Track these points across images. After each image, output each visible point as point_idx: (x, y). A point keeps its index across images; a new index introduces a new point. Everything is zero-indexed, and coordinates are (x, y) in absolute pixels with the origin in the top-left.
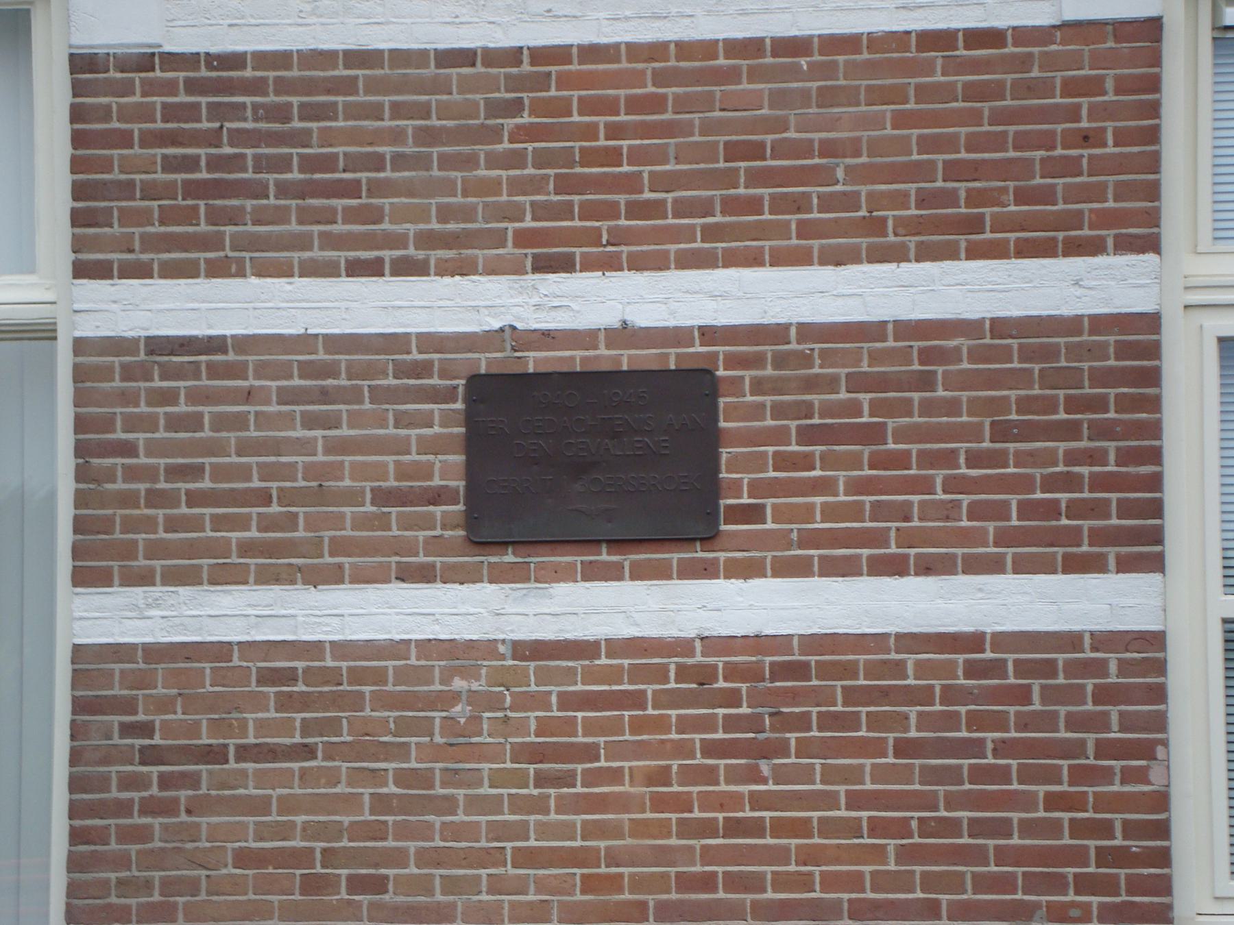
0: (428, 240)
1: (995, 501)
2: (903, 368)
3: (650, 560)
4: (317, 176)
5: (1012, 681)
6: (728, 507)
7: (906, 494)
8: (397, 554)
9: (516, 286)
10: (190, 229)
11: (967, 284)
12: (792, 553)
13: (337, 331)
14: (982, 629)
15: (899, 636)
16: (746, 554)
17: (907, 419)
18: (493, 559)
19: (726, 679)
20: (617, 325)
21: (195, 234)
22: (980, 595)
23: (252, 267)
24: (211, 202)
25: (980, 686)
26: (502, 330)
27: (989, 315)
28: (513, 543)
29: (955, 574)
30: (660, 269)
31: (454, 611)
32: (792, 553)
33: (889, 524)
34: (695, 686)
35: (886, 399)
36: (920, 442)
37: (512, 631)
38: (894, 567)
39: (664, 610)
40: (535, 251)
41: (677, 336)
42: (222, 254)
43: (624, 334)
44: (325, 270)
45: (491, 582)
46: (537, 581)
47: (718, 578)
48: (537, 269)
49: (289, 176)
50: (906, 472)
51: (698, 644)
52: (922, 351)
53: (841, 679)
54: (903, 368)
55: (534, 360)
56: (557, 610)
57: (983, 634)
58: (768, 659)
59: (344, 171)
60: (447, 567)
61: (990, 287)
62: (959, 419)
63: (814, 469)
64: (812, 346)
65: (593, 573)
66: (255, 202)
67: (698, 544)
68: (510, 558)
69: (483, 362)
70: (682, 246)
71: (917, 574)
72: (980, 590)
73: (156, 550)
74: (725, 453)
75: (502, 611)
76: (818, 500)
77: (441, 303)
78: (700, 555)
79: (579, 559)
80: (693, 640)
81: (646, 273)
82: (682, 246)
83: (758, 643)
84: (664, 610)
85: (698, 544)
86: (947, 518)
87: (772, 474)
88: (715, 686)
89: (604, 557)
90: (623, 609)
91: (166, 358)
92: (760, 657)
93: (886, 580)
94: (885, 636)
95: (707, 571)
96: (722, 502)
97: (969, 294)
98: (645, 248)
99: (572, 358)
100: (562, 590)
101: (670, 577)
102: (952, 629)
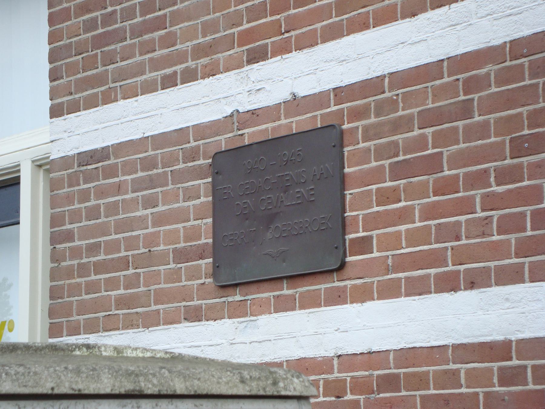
0: (200, 51)
1: (515, 214)
2: (452, 101)
3: (308, 291)
4: (148, 17)
5: (531, 387)
6: (351, 240)
7: (457, 215)
8: (184, 300)
9: (239, 77)
10: (94, 72)
11: (494, 13)
12: (389, 277)
13: (156, 132)
14: (509, 337)
15: (456, 347)
16: (361, 281)
17: (456, 147)
18: (230, 299)
19: (352, 393)
20: (289, 98)
21: (97, 74)
22: (507, 305)
23: (121, 93)
24: (103, 49)
25: (510, 393)
26: (232, 115)
27: (508, 39)
28: (287, 278)
29: (490, 286)
30: (312, 46)
31: (210, 343)
32: (389, 277)
33: (446, 244)
34: (333, 399)
35: (442, 130)
36: (464, 166)
37: (239, 357)
38: (449, 284)
39: (316, 333)
40: (247, 47)
41: (318, 100)
42: (107, 87)
43: (295, 104)
44: (149, 88)
45: (229, 318)
46: (252, 315)
47: (347, 303)
48: (250, 62)
49: (135, 21)
50: (456, 195)
51: (335, 362)
52: (467, 81)
53: (418, 390)
54: (452, 101)
55: (250, 134)
56: (260, 338)
57: (511, 341)
58: (376, 373)
59: (160, 10)
60: (210, 307)
61: (509, 12)
62: (489, 141)
63: (400, 201)
64: (397, 92)
65: (284, 305)
66: (121, 44)
67: (285, 282)
68: (238, 298)
69: (223, 141)
70: (325, 23)
71: (466, 289)
72: (507, 300)
73: (83, 308)
74: (206, 199)
75: (233, 342)
76: (403, 228)
77: (204, 100)
78: (337, 284)
79: (272, 294)
80: (332, 358)
81: (305, 51)
82: (325, 23)
83: (372, 358)
84: (316, 333)
85: (335, 274)
86: (483, 235)
87: (376, 209)
88: (345, 398)
89: (286, 292)
90: (294, 335)
91: (85, 168)
92: (371, 372)
93: (446, 295)
94: (443, 348)
95: (337, 298)
96: (347, 237)
97: (495, 22)
98: (304, 30)
99: (267, 129)
100: (264, 320)
101: (320, 306)
102: (488, 339)
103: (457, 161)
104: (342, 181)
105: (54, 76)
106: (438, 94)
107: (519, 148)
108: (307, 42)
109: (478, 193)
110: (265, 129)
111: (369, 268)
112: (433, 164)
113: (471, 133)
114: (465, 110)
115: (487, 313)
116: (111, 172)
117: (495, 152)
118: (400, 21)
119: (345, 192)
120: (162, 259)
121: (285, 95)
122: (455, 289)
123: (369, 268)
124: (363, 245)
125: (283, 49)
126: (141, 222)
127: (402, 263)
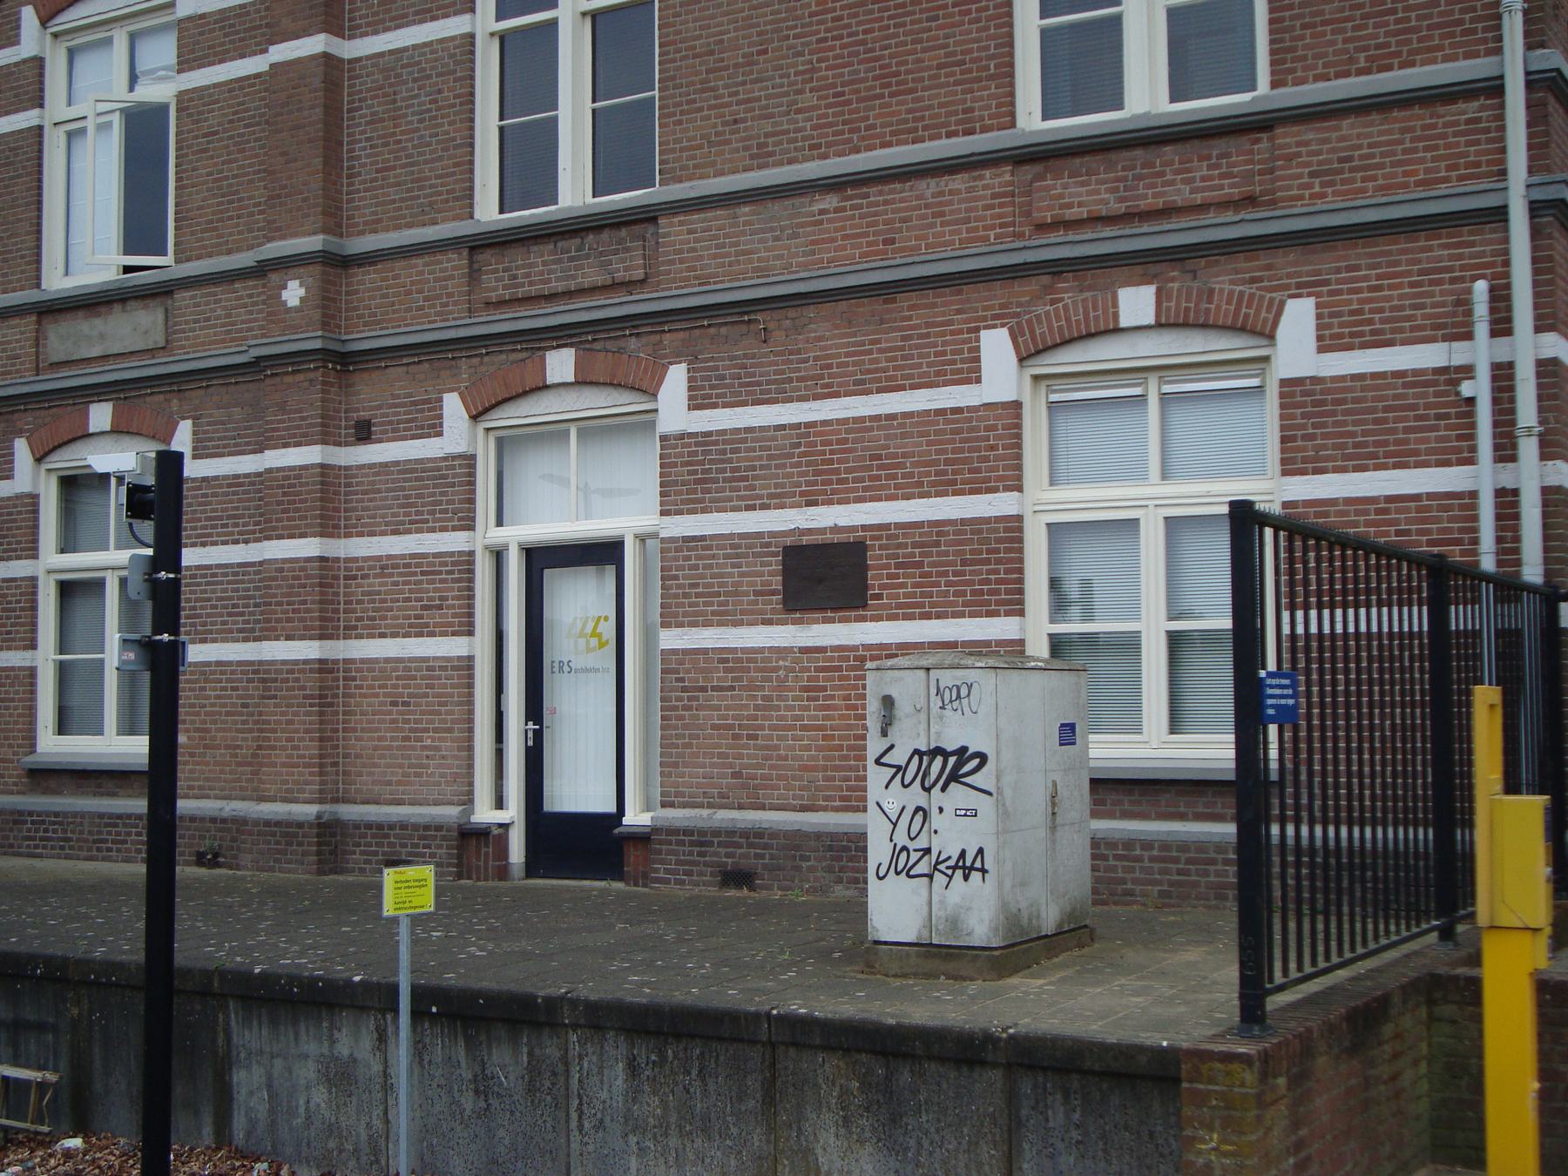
41: (853, 529)
43: (836, 529)
55: (805, 540)
69: (788, 541)
73: (685, 614)
74: (870, 573)
95: (863, 619)
103: (931, 565)
104: (865, 568)
105: (662, 494)
106: (921, 535)
107: (964, 563)
108: (846, 501)
109: (943, 580)
110: (819, 539)
111: (882, 607)
112: (920, 565)
113: (939, 554)
114: (937, 544)
115: (890, 663)
116: (709, 548)
117: (953, 563)
118: (1551, 902)
119: (150, 552)
120: (747, 594)
121: (831, 524)
122: (930, 618)
123: (882, 607)
124: (878, 597)
125: (830, 503)
126: (731, 575)
127: (899, 606)
